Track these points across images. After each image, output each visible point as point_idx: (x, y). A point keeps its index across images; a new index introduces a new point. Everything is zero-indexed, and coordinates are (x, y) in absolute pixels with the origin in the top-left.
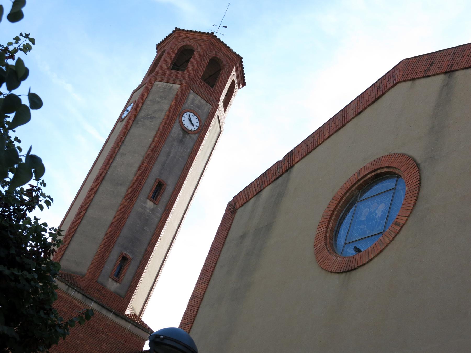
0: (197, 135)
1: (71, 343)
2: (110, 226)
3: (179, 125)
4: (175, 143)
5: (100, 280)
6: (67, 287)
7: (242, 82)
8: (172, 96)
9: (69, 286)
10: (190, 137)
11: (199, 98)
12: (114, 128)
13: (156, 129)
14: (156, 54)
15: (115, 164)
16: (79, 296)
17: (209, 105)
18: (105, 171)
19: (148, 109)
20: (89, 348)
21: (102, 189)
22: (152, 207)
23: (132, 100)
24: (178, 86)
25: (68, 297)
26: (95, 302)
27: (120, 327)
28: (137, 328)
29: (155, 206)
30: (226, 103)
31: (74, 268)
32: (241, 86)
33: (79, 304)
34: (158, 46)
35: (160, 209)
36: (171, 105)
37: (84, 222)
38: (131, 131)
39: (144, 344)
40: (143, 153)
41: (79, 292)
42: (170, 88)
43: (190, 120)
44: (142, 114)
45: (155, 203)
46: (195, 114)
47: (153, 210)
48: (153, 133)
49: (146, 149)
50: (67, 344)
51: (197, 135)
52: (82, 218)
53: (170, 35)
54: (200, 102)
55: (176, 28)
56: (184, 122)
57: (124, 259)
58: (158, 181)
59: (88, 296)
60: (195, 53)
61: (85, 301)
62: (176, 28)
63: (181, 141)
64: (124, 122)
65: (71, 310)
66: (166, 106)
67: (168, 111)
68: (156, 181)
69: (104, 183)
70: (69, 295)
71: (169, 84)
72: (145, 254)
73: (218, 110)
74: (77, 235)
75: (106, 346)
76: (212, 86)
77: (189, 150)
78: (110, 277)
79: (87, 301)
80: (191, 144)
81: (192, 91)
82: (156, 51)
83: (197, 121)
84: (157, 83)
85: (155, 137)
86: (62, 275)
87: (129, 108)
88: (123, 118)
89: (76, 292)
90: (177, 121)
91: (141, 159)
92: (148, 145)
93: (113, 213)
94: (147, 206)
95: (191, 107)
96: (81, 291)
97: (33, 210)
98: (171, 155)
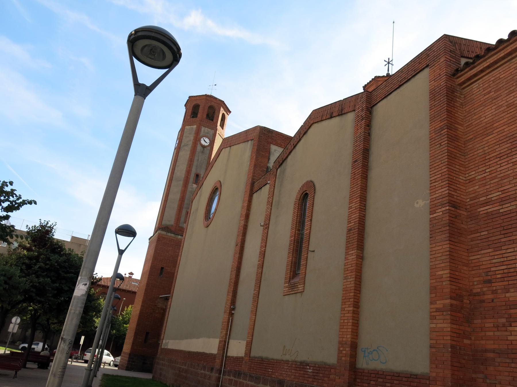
0: (210, 147)
5: (180, 225)
6: (166, 232)
7: (228, 111)
8: (194, 132)
9: (167, 232)
11: (207, 128)
13: (190, 150)
15: (176, 171)
16: (173, 235)
17: (212, 130)
19: (184, 141)
21: (172, 184)
23: (178, 138)
24: (196, 126)
26: (180, 235)
30: (222, 126)
31: (168, 223)
32: (229, 113)
34: (185, 105)
40: (186, 163)
41: (172, 233)
42: (192, 128)
43: (204, 141)
44: (182, 144)
45: (197, 185)
46: (206, 137)
48: (189, 152)
49: (187, 161)
51: (210, 147)
53: (188, 100)
54: (207, 130)
55: (189, 96)
56: (202, 143)
58: (196, 174)
59: (176, 234)
60: (200, 106)
61: (167, 233)
62: (189, 96)
63: (203, 152)
64: (176, 149)
66: (192, 138)
67: (193, 140)
68: (195, 174)
70: (168, 236)
71: (191, 126)
73: (217, 131)
74: (166, 208)
76: (212, 120)
77: (208, 155)
80: (208, 152)
81: (202, 127)
82: (185, 108)
83: (208, 140)
84: (186, 127)
85: (190, 154)
86: (163, 228)
87: (177, 143)
89: (171, 234)
90: (199, 143)
91: (186, 166)
93: (179, 194)
94: (194, 187)
96: (173, 233)
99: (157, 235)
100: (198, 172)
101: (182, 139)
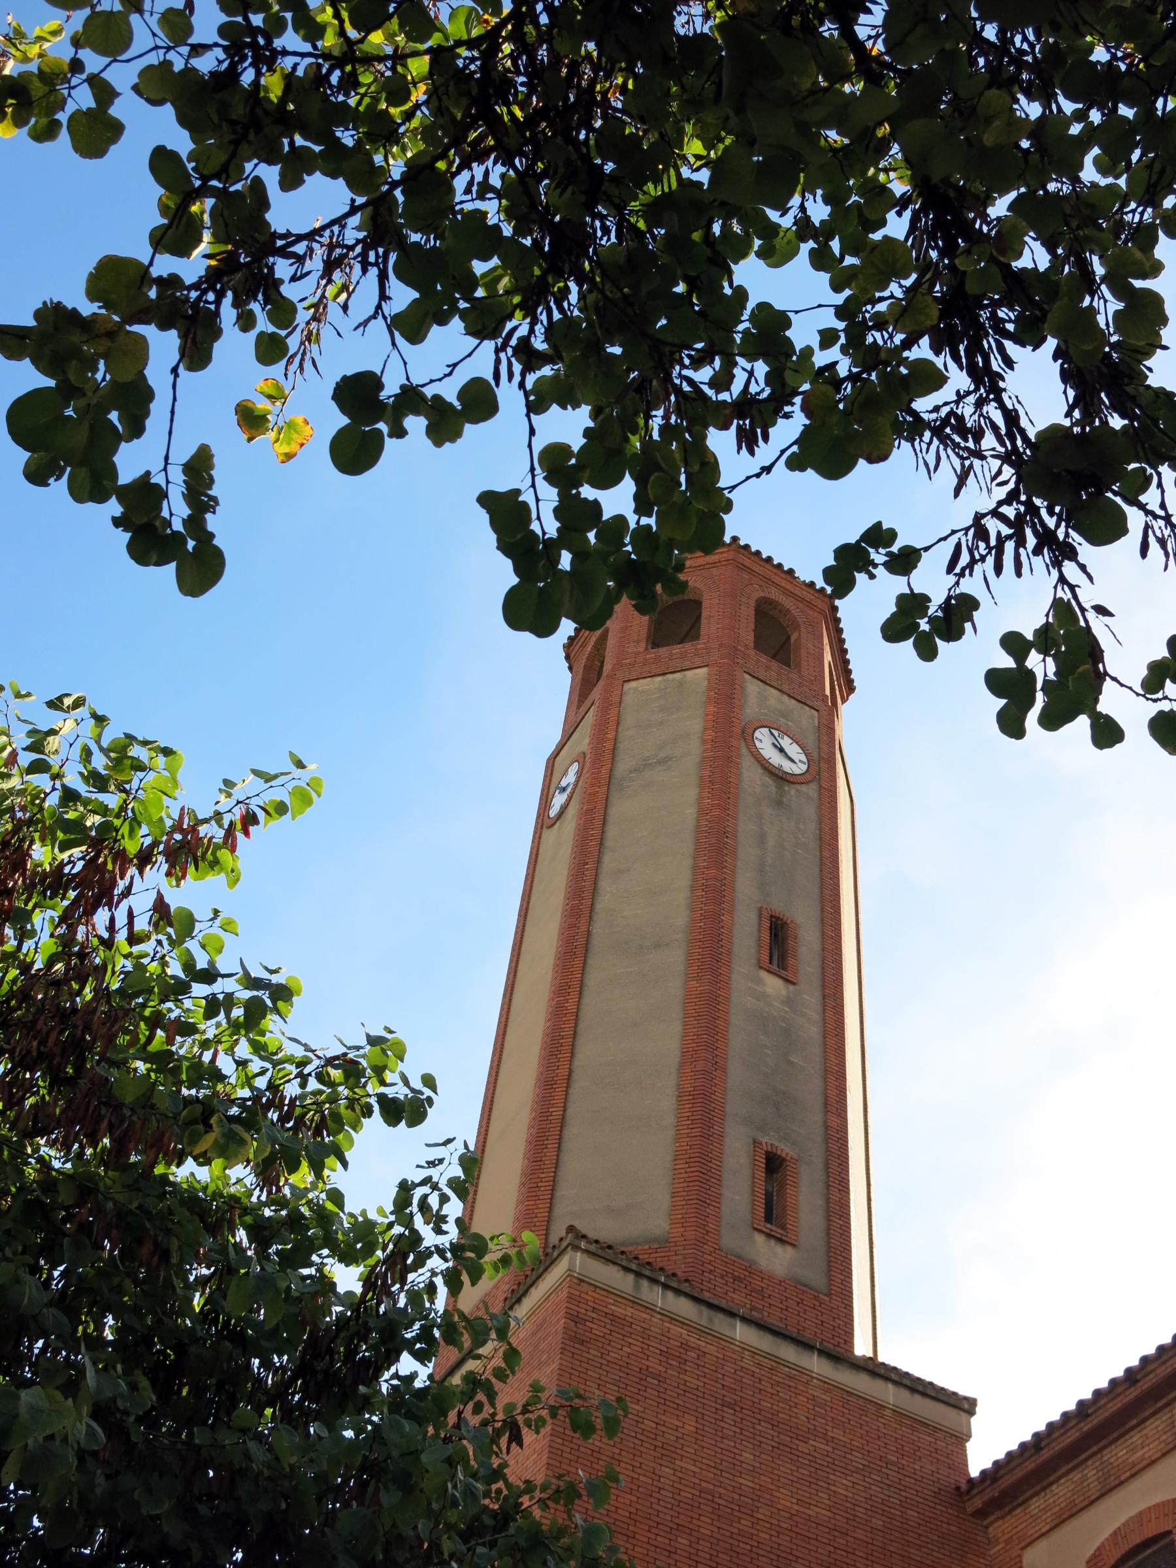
1: (721, 1490)
2: (682, 1065)
3: (752, 760)
4: (767, 810)
9: (638, 1274)
10: (798, 791)
12: (537, 855)
14: (567, 676)
16: (684, 1307)
18: (584, 928)
20: (795, 1501)
22: (784, 992)
25: (648, 1317)
26: (745, 1320)
27: (861, 1402)
28: (917, 1397)
29: (791, 988)
33: (693, 1340)
35: (811, 998)
36: (707, 715)
37: (579, 1085)
38: (613, 812)
39: (966, 1456)
41: (678, 1292)
44: (623, 766)
45: (787, 980)
47: (789, 1002)
48: (691, 794)
50: (710, 1498)
52: (569, 1075)
57: (774, 1164)
63: (779, 803)
65: (674, 1363)
68: (760, 916)
69: (593, 961)
70: (650, 1308)
72: (827, 1138)
74: (571, 1131)
75: (845, 1482)
78: (755, 1229)
79: (716, 1321)
88: (553, 813)
92: (691, 824)
93: (677, 1028)
94: (769, 990)
95: (765, 715)
97: (789, 339)
98: (771, 842)
99: (555, 1290)
100: (779, 906)
101: (616, 739)
